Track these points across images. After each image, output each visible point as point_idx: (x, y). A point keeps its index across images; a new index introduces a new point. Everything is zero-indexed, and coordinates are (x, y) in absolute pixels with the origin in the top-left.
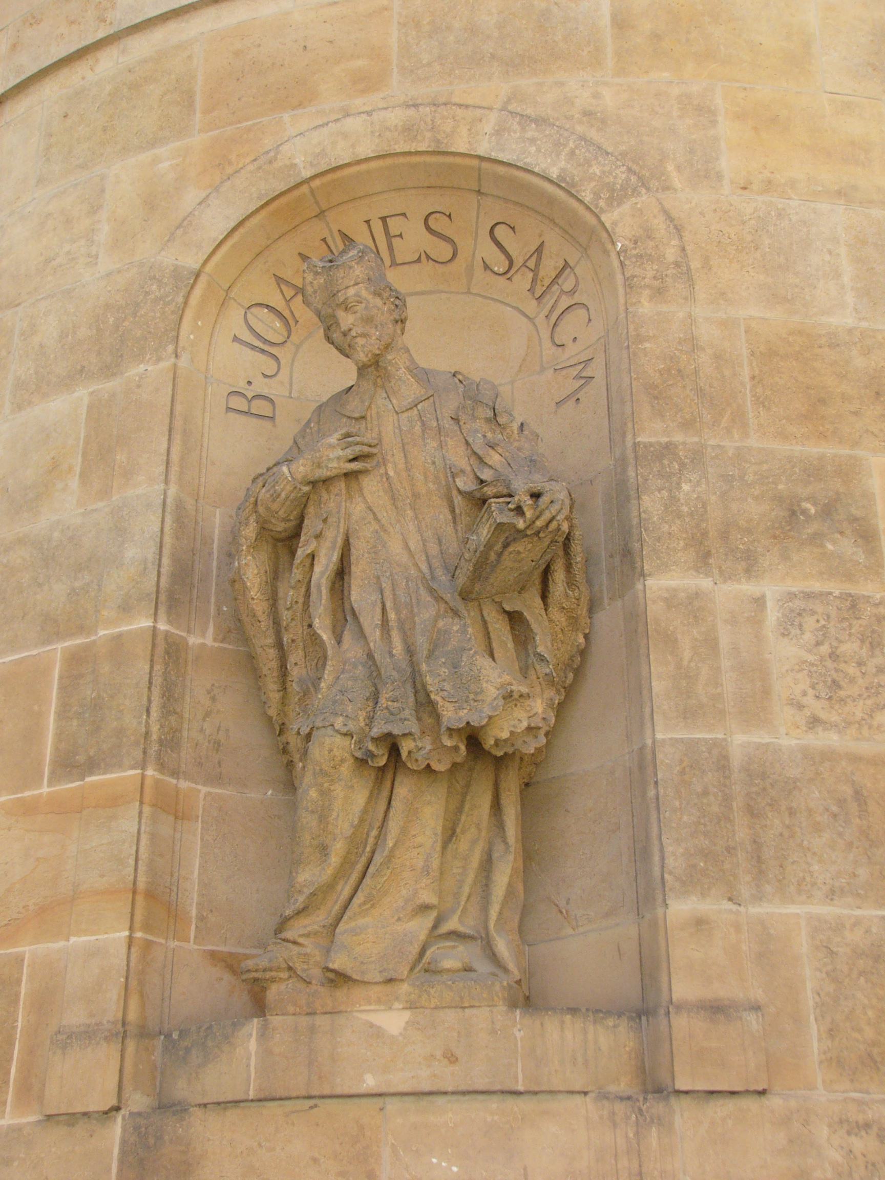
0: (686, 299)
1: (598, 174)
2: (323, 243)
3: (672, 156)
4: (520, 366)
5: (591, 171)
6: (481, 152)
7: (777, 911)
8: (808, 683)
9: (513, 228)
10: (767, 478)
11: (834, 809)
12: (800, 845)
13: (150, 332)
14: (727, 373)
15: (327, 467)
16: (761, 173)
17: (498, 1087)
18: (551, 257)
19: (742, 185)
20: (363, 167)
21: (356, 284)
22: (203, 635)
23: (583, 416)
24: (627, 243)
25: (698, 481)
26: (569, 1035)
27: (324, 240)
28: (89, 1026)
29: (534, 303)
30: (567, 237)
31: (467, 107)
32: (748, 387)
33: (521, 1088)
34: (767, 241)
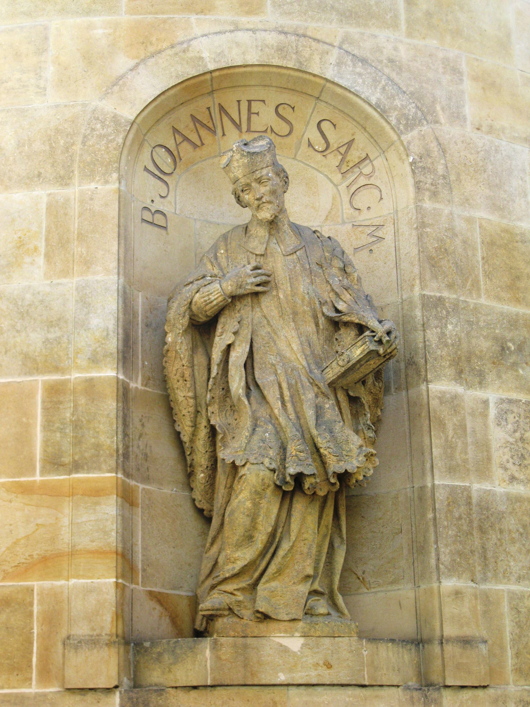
0: (449, 201)
1: (399, 106)
2: (207, 110)
3: (439, 100)
4: (327, 216)
5: (395, 104)
6: (328, 76)
7: (494, 588)
8: (510, 455)
9: (335, 126)
10: (490, 325)
11: (521, 530)
12: (505, 550)
13: (97, 160)
14: (470, 253)
15: (245, 288)
16: (487, 120)
17: (354, 682)
18: (357, 150)
19: (477, 127)
20: (248, 69)
21: (267, 167)
22: (136, 382)
23: (376, 263)
24: (416, 157)
25: (456, 324)
26: (391, 654)
27: (209, 108)
28: (92, 636)
29: (340, 176)
30: (372, 140)
31: (318, 41)
32: (481, 264)
33: (367, 683)
34: (490, 167)
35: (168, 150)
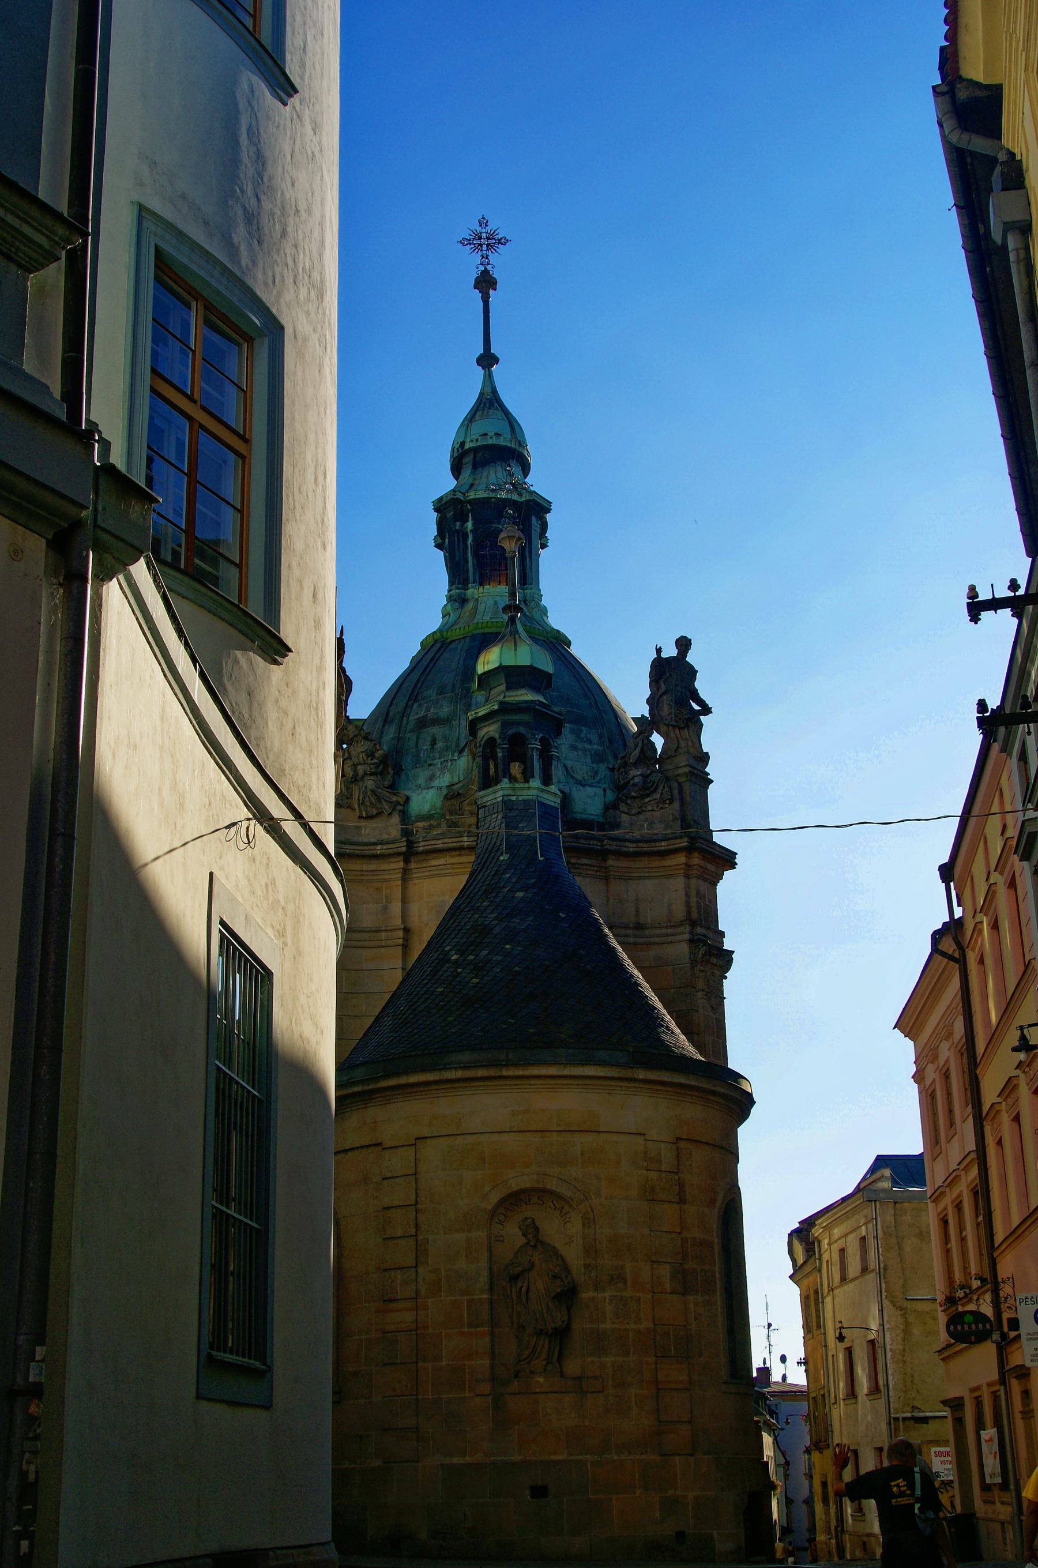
35: (503, 1214)
